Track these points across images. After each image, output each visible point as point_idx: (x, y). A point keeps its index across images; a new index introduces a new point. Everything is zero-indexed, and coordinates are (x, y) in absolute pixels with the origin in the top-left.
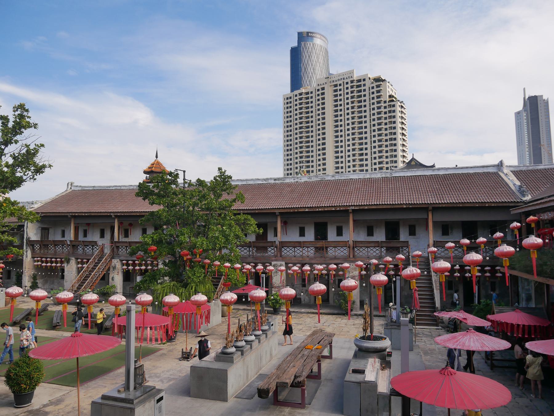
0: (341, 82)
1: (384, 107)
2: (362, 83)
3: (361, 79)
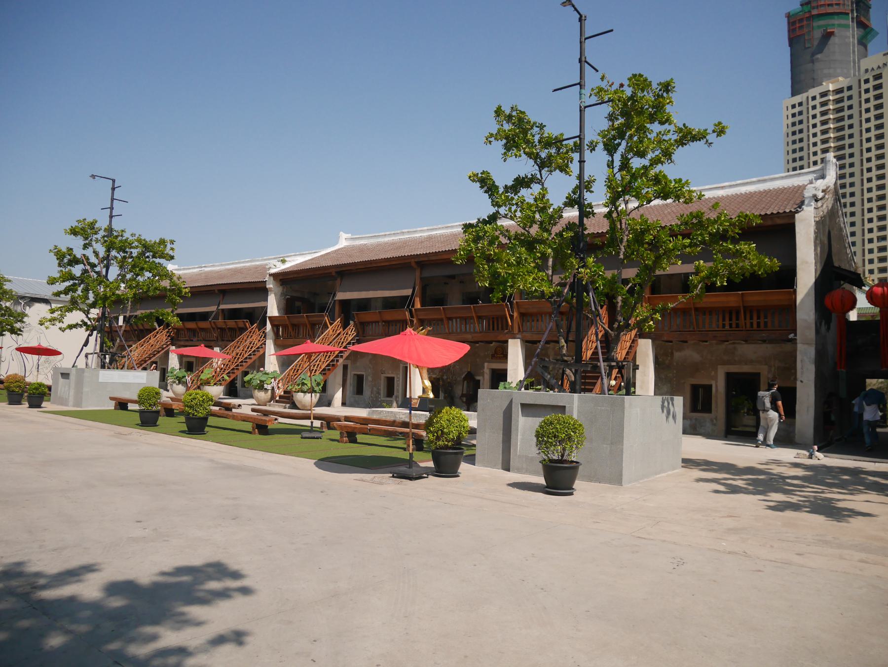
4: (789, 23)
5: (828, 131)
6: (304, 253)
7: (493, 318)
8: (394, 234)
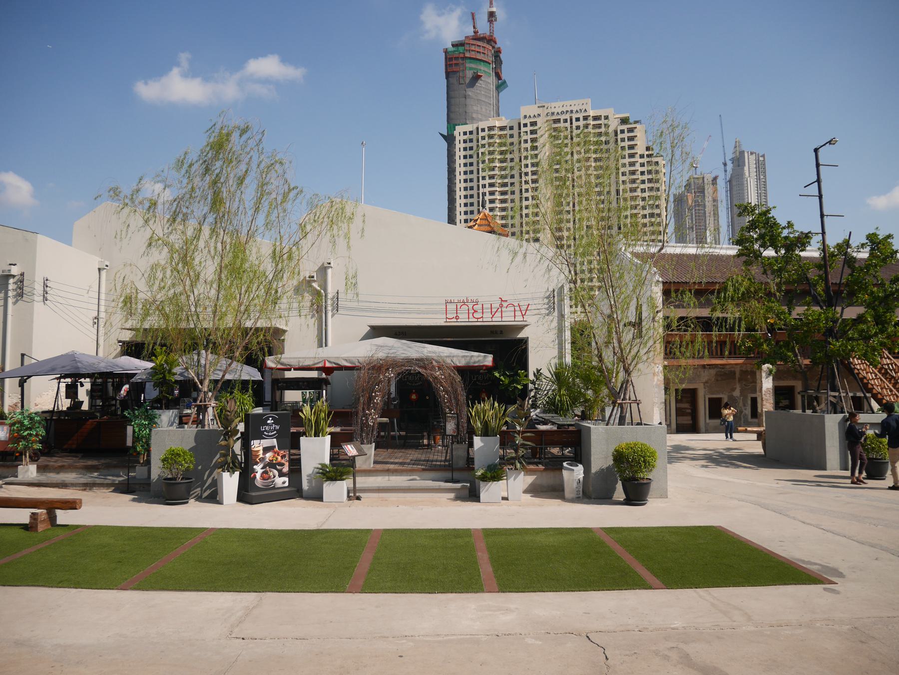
0: (567, 117)
1: (640, 155)
2: (602, 121)
3: (601, 116)
4: (446, 58)
5: (634, 164)
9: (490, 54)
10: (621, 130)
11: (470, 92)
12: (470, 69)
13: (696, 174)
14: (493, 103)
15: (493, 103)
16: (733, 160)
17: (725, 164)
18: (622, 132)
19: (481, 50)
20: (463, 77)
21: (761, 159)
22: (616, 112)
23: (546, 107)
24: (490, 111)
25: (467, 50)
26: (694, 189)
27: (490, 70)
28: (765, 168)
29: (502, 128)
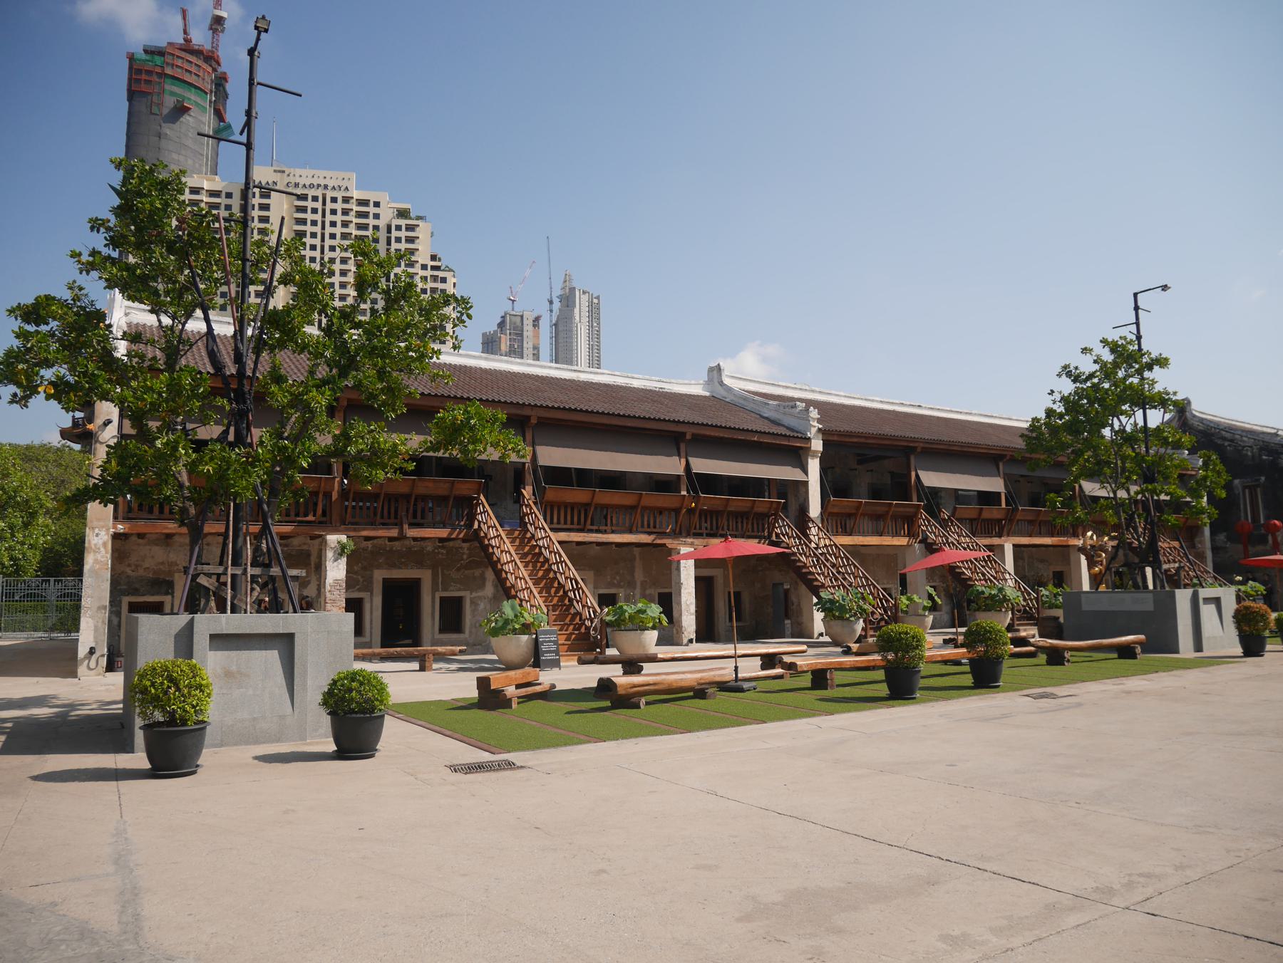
0: (319, 193)
1: (422, 265)
2: (372, 210)
4: (131, 68)
6: (636, 376)
7: (864, 532)
8: (801, 389)
9: (208, 79)
10: (396, 226)
11: (168, 129)
12: (171, 94)
13: (513, 310)
14: (207, 155)
15: (207, 155)
16: (561, 298)
17: (551, 302)
18: (398, 228)
19: (194, 69)
20: (159, 104)
21: (595, 301)
22: (393, 199)
23: (287, 173)
24: (200, 165)
25: (168, 64)
26: (510, 330)
27: (206, 101)
28: (599, 314)
29: (214, 194)
